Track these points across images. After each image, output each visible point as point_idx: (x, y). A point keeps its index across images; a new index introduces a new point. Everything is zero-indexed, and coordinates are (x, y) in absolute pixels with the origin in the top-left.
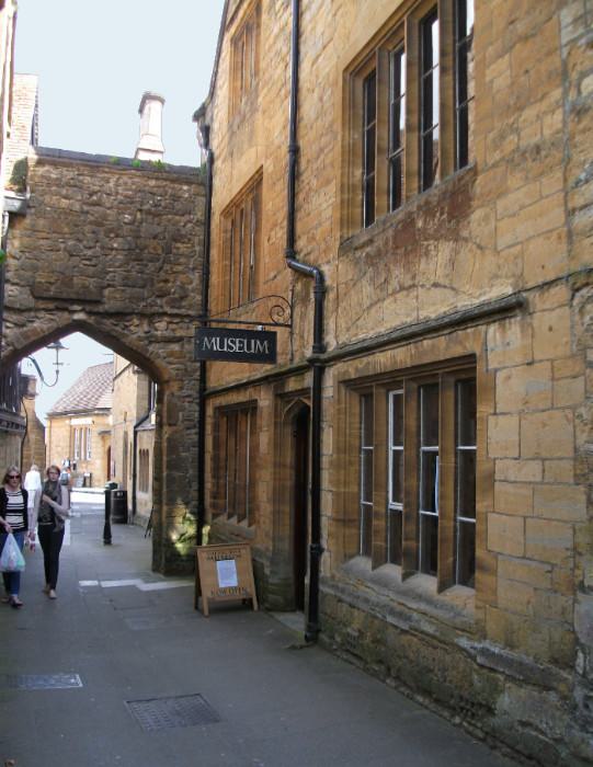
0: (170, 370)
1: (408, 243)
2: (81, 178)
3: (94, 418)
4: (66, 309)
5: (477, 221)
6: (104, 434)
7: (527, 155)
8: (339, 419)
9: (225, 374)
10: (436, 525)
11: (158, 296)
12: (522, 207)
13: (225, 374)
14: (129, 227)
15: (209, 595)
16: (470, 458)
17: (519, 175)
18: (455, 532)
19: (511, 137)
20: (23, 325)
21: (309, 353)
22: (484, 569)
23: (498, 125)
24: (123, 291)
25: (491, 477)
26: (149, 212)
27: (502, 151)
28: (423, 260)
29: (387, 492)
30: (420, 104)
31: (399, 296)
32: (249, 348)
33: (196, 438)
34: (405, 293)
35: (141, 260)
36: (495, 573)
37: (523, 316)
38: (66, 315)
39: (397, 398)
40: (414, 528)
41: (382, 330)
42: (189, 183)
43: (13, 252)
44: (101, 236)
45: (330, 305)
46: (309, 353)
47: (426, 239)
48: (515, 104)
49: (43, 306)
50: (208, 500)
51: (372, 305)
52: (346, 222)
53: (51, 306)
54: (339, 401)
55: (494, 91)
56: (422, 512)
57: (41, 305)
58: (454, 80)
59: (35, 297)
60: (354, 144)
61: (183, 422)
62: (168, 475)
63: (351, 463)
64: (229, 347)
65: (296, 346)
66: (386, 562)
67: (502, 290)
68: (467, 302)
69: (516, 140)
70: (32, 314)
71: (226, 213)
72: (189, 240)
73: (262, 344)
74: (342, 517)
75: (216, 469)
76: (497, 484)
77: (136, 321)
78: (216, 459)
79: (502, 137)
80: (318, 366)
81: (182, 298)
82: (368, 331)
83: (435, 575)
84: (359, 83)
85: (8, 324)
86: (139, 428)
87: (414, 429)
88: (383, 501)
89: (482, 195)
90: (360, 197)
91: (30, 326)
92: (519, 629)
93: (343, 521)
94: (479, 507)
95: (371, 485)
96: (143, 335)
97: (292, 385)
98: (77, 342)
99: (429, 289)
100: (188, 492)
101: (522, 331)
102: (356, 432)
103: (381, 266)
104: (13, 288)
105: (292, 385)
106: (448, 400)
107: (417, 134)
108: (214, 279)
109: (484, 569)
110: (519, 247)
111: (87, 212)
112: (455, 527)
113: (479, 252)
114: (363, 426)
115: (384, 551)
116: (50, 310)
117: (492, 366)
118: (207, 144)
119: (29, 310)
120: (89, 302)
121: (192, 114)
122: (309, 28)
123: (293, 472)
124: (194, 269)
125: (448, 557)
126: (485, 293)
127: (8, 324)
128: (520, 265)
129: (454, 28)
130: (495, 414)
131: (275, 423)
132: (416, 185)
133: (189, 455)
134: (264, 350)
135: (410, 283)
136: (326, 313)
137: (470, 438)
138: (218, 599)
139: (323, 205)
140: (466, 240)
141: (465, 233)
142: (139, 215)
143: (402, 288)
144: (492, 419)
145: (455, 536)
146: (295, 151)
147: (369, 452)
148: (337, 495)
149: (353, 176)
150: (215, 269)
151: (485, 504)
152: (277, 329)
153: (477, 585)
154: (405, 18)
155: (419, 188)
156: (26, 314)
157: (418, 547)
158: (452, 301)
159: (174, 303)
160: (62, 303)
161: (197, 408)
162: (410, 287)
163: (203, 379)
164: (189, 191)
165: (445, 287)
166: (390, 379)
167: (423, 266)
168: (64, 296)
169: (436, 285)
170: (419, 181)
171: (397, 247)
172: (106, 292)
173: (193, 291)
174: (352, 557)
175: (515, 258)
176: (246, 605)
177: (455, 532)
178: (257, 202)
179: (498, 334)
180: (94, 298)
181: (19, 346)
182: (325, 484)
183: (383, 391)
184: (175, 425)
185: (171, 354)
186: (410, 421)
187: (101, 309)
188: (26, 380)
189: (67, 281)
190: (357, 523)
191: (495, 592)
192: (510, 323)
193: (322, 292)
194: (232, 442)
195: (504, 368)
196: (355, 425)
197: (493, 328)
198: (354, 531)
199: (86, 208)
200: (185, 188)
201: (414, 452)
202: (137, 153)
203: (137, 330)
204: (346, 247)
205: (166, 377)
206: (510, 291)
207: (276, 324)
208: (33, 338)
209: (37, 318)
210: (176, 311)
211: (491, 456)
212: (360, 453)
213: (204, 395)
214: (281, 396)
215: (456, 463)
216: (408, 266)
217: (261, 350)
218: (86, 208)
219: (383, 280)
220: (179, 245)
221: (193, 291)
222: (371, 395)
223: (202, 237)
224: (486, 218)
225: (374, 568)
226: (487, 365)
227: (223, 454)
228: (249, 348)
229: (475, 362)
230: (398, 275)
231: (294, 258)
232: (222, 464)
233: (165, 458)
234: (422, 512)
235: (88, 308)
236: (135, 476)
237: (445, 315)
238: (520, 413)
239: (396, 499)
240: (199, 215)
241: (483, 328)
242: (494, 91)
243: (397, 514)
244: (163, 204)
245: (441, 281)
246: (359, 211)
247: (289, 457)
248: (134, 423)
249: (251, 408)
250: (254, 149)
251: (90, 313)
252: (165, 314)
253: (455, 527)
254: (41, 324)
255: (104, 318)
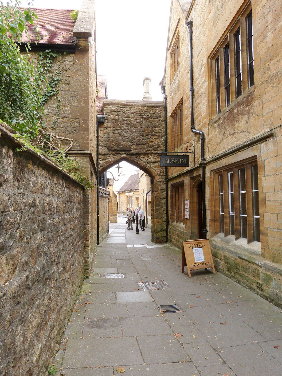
0: (155, 172)
1: (232, 118)
2: (122, 108)
3: (134, 193)
4: (119, 154)
5: (256, 105)
6: (137, 198)
7: (273, 77)
8: (211, 184)
9: (174, 171)
10: (246, 220)
11: (150, 147)
12: (272, 97)
13: (174, 171)
14: (139, 124)
15: (191, 266)
16: (257, 193)
17: (271, 86)
18: (253, 222)
19: (267, 71)
20: (105, 160)
21: (200, 161)
22: (263, 234)
23: (262, 68)
24: (138, 146)
25: (264, 200)
26: (145, 119)
27: (264, 77)
28: (237, 123)
29: (229, 209)
30: (235, 66)
31: (230, 137)
32: (179, 161)
33: (165, 195)
34: (231, 136)
35: (144, 135)
36: (267, 235)
37: (274, 139)
38: (119, 155)
39: (231, 175)
40: (239, 221)
41: (224, 151)
42: (158, 107)
43: (101, 135)
44: (130, 127)
45: (207, 144)
46: (200, 161)
47: (238, 116)
48: (268, 59)
49: (111, 153)
50: (170, 217)
51: (220, 142)
52: (211, 113)
53: (114, 152)
54: (211, 178)
55: (261, 55)
56: (242, 215)
57: (110, 152)
58: (247, 54)
59: (109, 150)
60: (212, 85)
61: (160, 190)
62: (156, 209)
63: (216, 199)
64: (172, 161)
65: (195, 160)
66: (230, 234)
67: (264, 131)
68: (254, 136)
69: (269, 72)
70: (108, 156)
71: (172, 116)
72: (160, 127)
73: (184, 160)
74: (213, 219)
75: (172, 206)
76: (266, 202)
77: (143, 156)
78: (172, 202)
79: (264, 72)
80: (203, 166)
81: (158, 147)
82: (220, 151)
83: (247, 238)
84: (214, 62)
85: (100, 160)
86: (148, 194)
87: (237, 185)
88: (228, 212)
89: (257, 96)
90: (216, 103)
91: (108, 160)
92: (277, 256)
93: (214, 220)
94: (261, 211)
95: (224, 206)
96: (145, 161)
97: (195, 174)
98: (124, 164)
99: (240, 133)
100: (163, 214)
101: (274, 144)
102: (217, 188)
103: (223, 128)
104: (101, 147)
105: (195, 174)
106: (249, 174)
107: (234, 77)
108: (169, 140)
109: (263, 234)
110: (271, 113)
111: (124, 120)
112: (253, 219)
113: (257, 117)
114: (220, 186)
115: (229, 230)
116: (114, 154)
117: (263, 159)
118: (164, 93)
119: (107, 154)
120: (127, 150)
121: (159, 83)
122: (195, 43)
123: (197, 205)
124: (162, 137)
125: (251, 232)
126: (259, 132)
127: (100, 160)
128: (272, 120)
129: (247, 34)
130: (265, 176)
131: (190, 188)
132: (235, 96)
133: (163, 201)
134: (185, 162)
135: (233, 132)
136: (205, 147)
137: (257, 188)
138: (195, 268)
139: (203, 107)
140: (252, 113)
141: (251, 111)
142: (142, 119)
143: (230, 134)
144: (263, 178)
145: (253, 223)
146: (193, 91)
147: (222, 195)
148: (211, 211)
149: (213, 96)
150: (169, 136)
151: (263, 210)
152: (189, 154)
153: (261, 240)
154: (228, 34)
155: (236, 97)
156: (106, 156)
157: (240, 228)
158: (248, 137)
159: (154, 149)
160: (117, 151)
161: (165, 185)
162: (233, 134)
163: (167, 175)
164: (158, 110)
165: (245, 132)
166: (228, 168)
167: (237, 125)
168: (118, 149)
169: (242, 132)
170: (236, 95)
171: (228, 120)
172: (132, 147)
173: (162, 145)
174: (217, 233)
175: (270, 117)
176: (206, 272)
177: (253, 222)
178: (181, 111)
179: (264, 147)
180: (129, 149)
181: (104, 167)
182: (207, 208)
183: (226, 172)
184: (157, 191)
185: (155, 167)
186: (236, 182)
187: (131, 152)
188: (108, 180)
189: (119, 144)
190: (219, 221)
191: (268, 242)
192: (269, 142)
193: (203, 140)
194: (177, 196)
195: (267, 159)
196: (217, 186)
197: (263, 144)
198: (218, 224)
199: (124, 119)
200: (157, 109)
201: (237, 194)
202: (143, 99)
203: (143, 160)
204: (211, 123)
205: (154, 175)
206: (268, 130)
207: (189, 153)
208: (109, 164)
209: (110, 157)
210: (156, 152)
211: (264, 192)
212: (219, 196)
213: (167, 181)
214: (192, 179)
215: (253, 196)
216: (232, 126)
217: (184, 162)
218: (124, 119)
219: (224, 132)
220: (156, 129)
221: (162, 145)
222: (222, 174)
223: (164, 126)
224: (259, 104)
225: (225, 236)
226: (261, 159)
227: (174, 200)
228: (179, 161)
229: (257, 158)
230: (229, 130)
231: (194, 128)
232: (174, 204)
233: (155, 203)
234: (242, 215)
235: (127, 152)
236: (147, 211)
237: (246, 142)
238: (274, 176)
239: (232, 211)
240: (163, 118)
241: (259, 145)
242: (261, 55)
243: (232, 216)
244: (150, 115)
245: (244, 130)
246: (216, 109)
247: (196, 200)
248: (146, 193)
249: (182, 184)
250: (179, 92)
251: (127, 154)
252: (152, 153)
253: (253, 219)
254: (111, 159)
255: (132, 156)
